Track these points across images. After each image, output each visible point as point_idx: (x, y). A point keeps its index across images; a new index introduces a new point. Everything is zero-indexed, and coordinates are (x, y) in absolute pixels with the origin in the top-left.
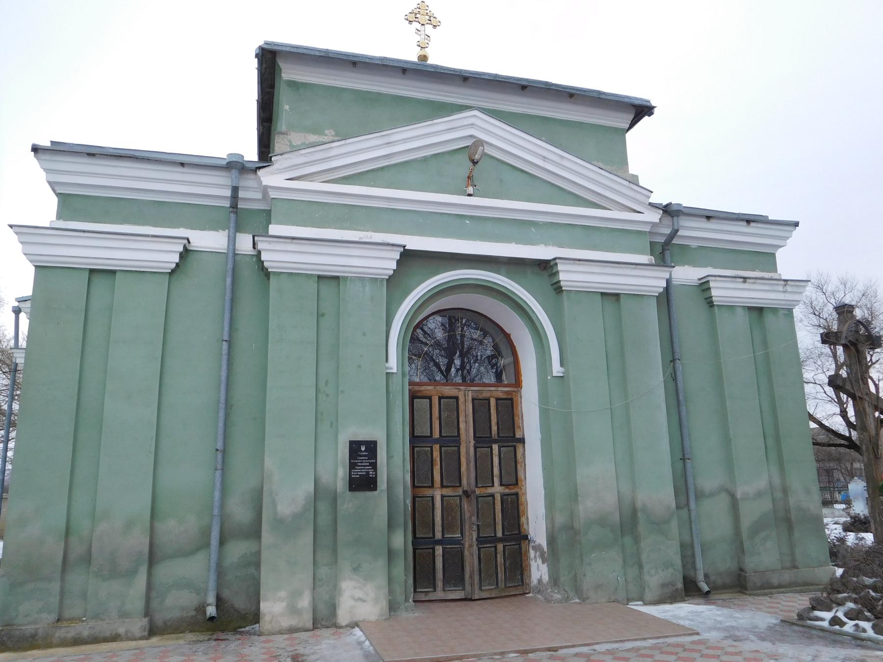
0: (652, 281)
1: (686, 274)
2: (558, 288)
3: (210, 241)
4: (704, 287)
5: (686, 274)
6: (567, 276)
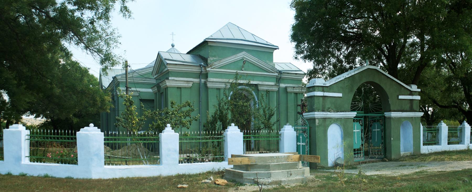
0: (276, 89)
1: (283, 85)
2: (258, 90)
3: (197, 80)
4: (286, 88)
5: (283, 85)
6: (260, 88)
